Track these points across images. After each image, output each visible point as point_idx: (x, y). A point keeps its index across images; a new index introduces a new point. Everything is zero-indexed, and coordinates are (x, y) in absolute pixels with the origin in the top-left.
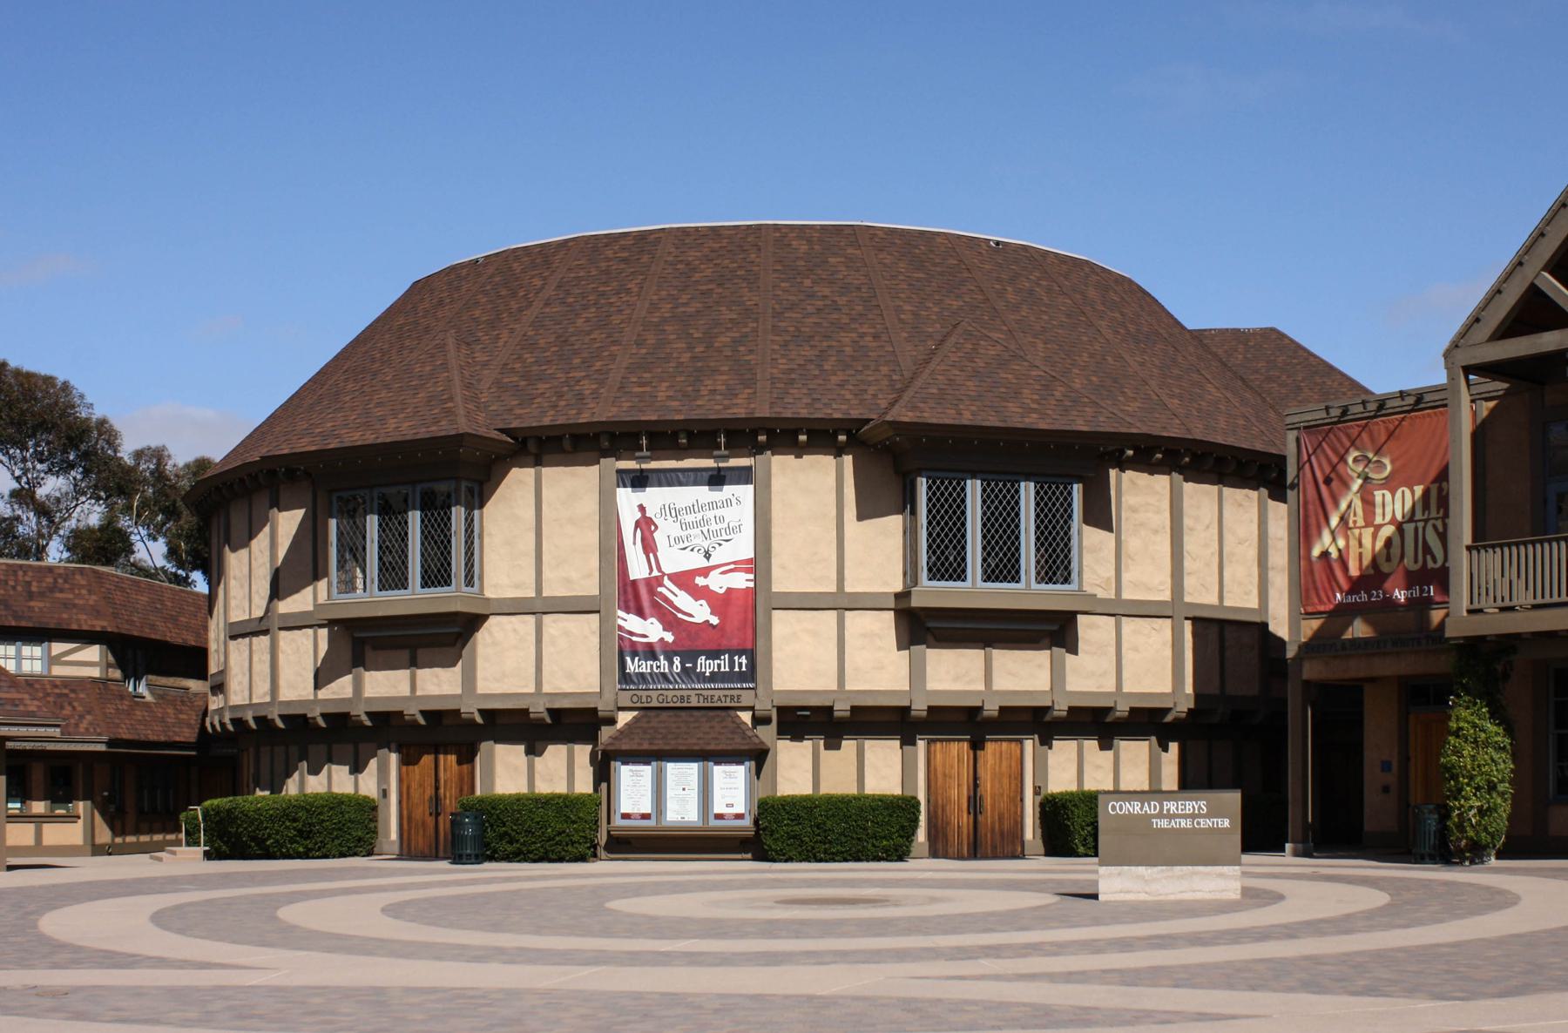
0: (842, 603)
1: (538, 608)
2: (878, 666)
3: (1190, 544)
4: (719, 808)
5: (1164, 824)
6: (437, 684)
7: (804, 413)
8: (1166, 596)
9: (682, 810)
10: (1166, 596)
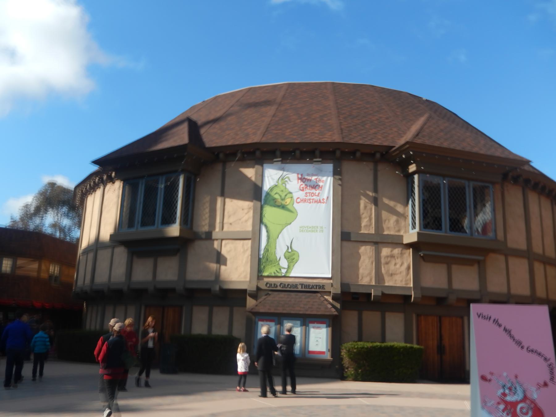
6: (167, 272)
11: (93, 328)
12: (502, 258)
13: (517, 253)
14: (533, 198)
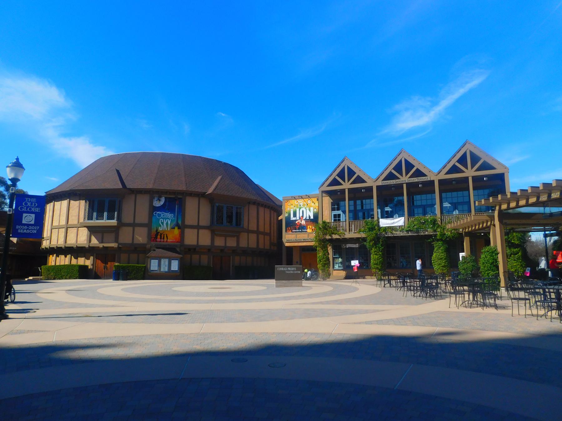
0: (198, 227)
1: (134, 225)
2: (205, 239)
3: (260, 220)
4: (172, 269)
5: (288, 272)
7: (194, 190)
8: (256, 229)
9: (164, 268)
10: (256, 229)
11: (62, 263)
12: (246, 234)
13: (253, 232)
14: (261, 210)
